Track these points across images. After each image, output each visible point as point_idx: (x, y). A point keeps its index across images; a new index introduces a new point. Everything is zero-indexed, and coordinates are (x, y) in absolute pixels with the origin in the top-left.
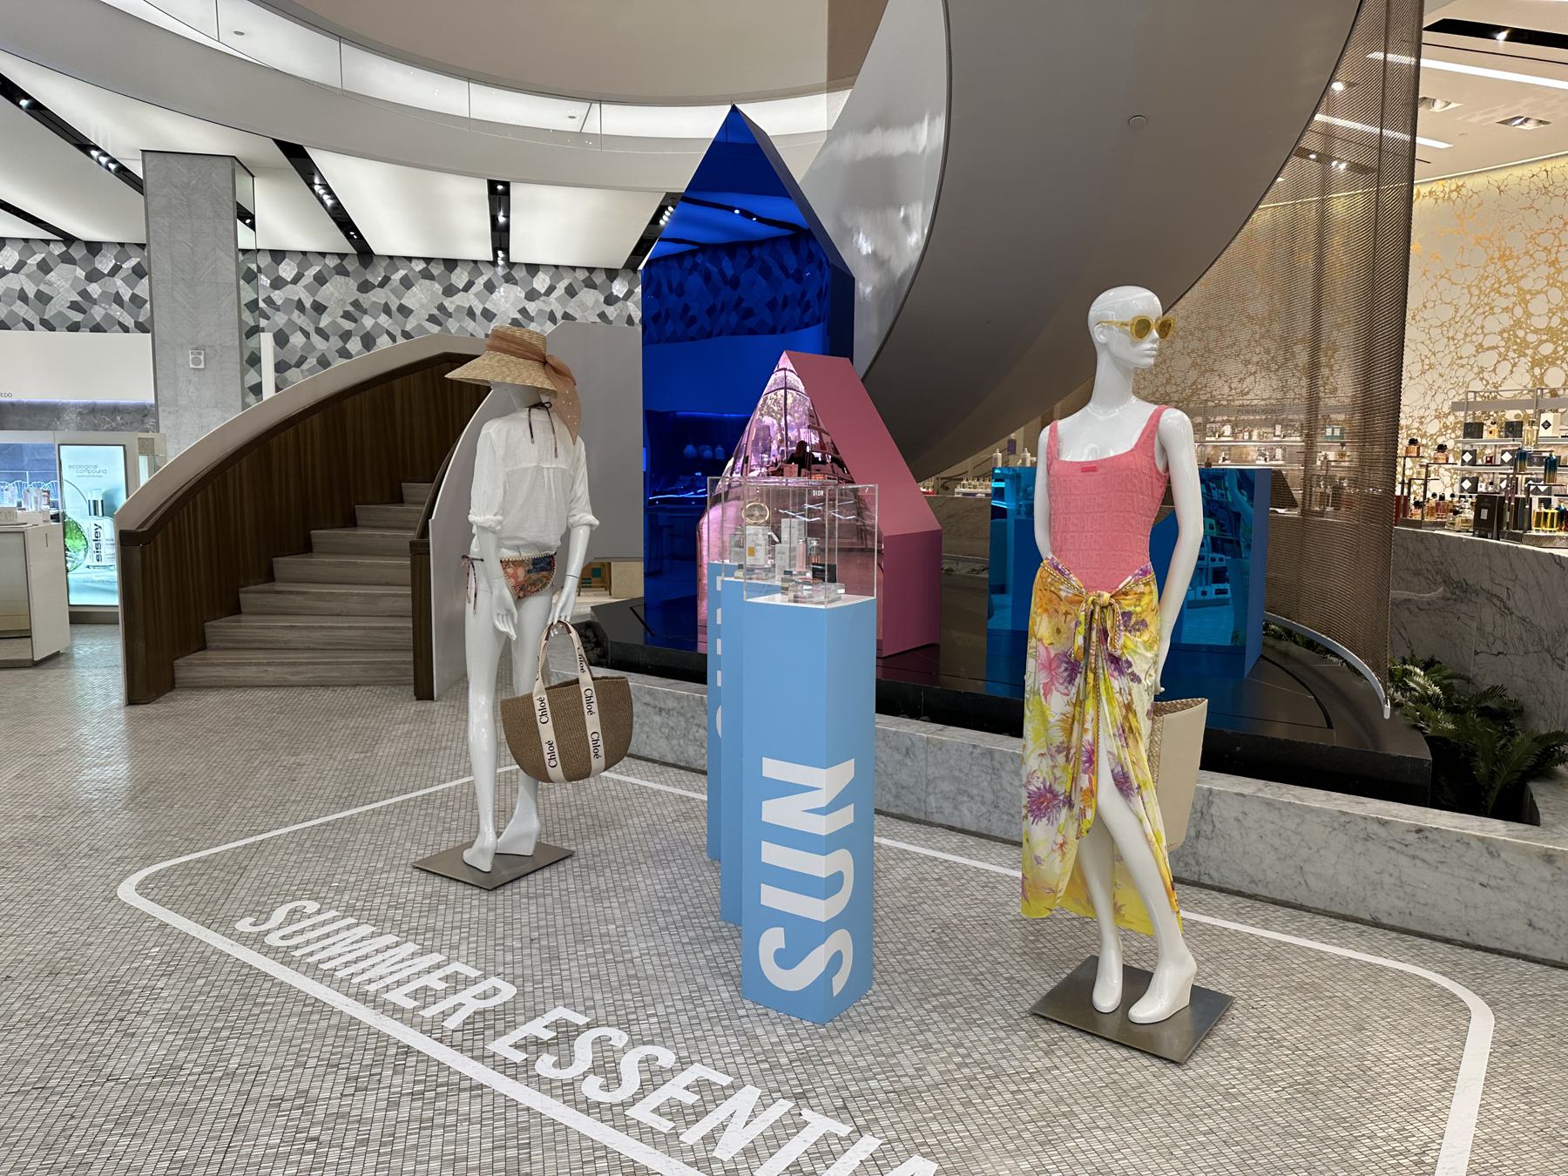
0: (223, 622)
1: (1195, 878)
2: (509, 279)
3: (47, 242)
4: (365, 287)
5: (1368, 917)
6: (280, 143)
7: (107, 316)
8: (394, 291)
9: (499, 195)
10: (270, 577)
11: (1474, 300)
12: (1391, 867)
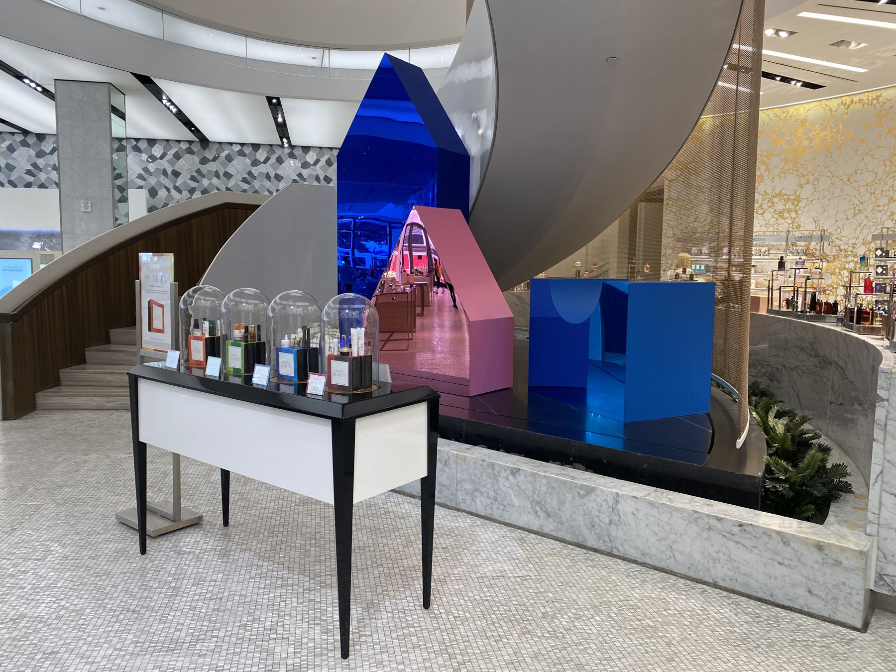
0: (66, 370)
1: (609, 550)
2: (292, 156)
3: (13, 134)
4: (204, 161)
5: (711, 581)
6: (137, 76)
7: (48, 179)
8: (221, 163)
9: (275, 105)
10: (107, 341)
11: (888, 169)
12: (724, 549)
